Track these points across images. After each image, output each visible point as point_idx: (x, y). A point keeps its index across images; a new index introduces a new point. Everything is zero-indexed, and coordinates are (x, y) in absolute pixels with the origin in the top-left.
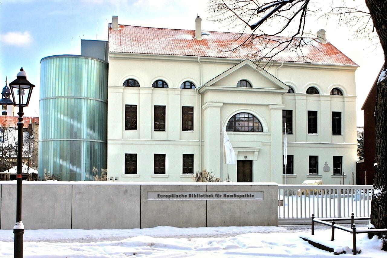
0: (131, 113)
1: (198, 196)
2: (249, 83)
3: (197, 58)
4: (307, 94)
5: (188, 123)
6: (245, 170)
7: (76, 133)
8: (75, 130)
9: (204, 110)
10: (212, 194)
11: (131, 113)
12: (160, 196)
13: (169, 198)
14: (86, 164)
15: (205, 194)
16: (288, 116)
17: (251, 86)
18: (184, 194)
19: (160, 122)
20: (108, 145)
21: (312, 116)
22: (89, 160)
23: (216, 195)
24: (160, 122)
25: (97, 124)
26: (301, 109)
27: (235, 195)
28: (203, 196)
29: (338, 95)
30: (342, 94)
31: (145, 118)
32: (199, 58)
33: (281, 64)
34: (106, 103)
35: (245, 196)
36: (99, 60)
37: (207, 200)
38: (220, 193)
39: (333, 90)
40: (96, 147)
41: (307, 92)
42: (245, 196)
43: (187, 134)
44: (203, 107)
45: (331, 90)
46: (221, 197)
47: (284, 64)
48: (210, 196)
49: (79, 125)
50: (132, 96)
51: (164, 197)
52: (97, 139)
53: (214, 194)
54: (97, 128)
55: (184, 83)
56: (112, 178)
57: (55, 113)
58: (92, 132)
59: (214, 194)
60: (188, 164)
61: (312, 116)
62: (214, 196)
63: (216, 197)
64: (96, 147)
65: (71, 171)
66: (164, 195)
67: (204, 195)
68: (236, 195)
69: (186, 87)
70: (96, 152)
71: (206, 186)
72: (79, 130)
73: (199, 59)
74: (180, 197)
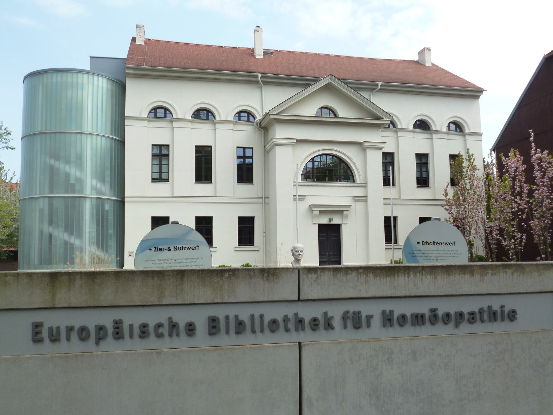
0: (161, 154)
1: (257, 327)
2: (333, 112)
3: (257, 77)
4: (415, 130)
5: (245, 173)
6: (330, 237)
7: (73, 185)
8: (72, 181)
9: (268, 152)
10: (326, 314)
11: (161, 154)
12: (45, 334)
13: (97, 343)
14: (90, 232)
15: (290, 311)
16: (388, 159)
17: (335, 115)
18: (182, 317)
19: (204, 169)
20: (126, 205)
21: (422, 161)
22: (95, 226)
23: (345, 317)
24: (204, 169)
25: (108, 173)
26: (407, 148)
27: (433, 311)
28: (282, 324)
29: (456, 130)
30: (461, 130)
31: (183, 164)
32: (260, 75)
33: (377, 85)
34: (122, 143)
35: (478, 317)
36: (113, 81)
37: (300, 343)
38: (366, 309)
39: (449, 124)
40: (107, 207)
41: (415, 126)
42: (478, 317)
43: (245, 188)
44: (267, 147)
45: (447, 125)
46: (368, 326)
47: (381, 86)
48: (315, 324)
49: (78, 174)
50: (159, 133)
51: (68, 339)
52: (109, 195)
53: (336, 312)
54: (108, 179)
55: (239, 113)
56: (132, 254)
57: (41, 156)
58: (99, 185)
59: (336, 312)
60: (246, 231)
61: (422, 161)
62: (337, 323)
63: (345, 327)
64: (107, 207)
65: (66, 243)
66: (70, 329)
67: (286, 319)
68: (440, 313)
69: (242, 119)
70: (107, 215)
71: (297, 271)
72: (80, 181)
73: (260, 78)
74: (159, 336)
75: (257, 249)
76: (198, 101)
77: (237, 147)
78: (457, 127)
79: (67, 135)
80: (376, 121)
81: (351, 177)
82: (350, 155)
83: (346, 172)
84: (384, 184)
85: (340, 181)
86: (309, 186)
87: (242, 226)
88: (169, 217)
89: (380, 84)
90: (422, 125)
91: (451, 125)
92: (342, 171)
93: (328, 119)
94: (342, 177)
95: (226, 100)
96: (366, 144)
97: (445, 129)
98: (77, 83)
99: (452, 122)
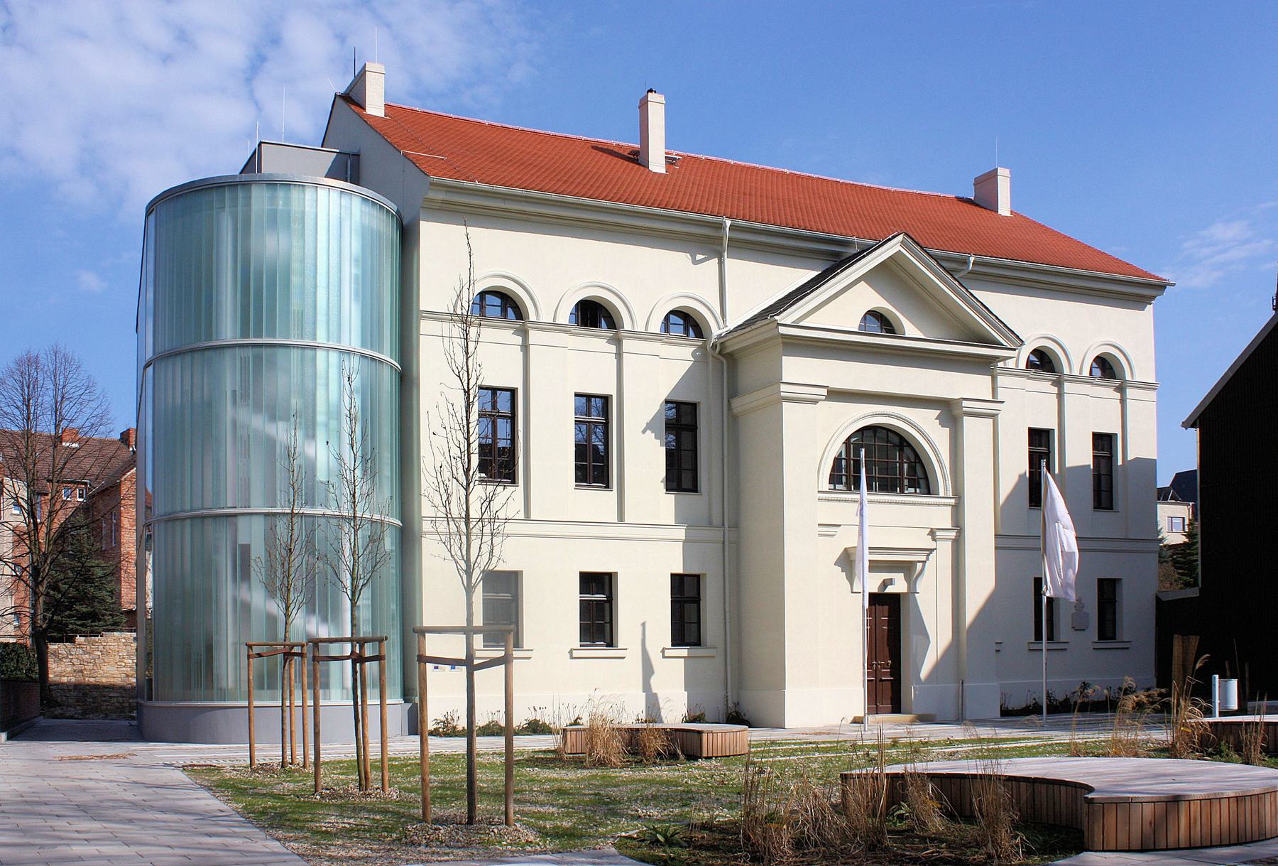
33: (966, 262)
39: (667, 318)
50: (497, 355)
75: (1062, 646)
76: (608, 283)
77: (576, 395)
78: (1106, 367)
79: (281, 351)
80: (976, 348)
81: (922, 482)
82: (926, 429)
83: (912, 469)
84: (1030, 502)
85: (902, 491)
86: (846, 501)
87: (588, 597)
88: (672, 575)
89: (972, 259)
90: (592, 314)
91: (673, 319)
92: (906, 466)
93: (878, 340)
94: (906, 482)
95: (650, 278)
96: (965, 403)
97: (656, 326)
98: (288, 213)
99: (673, 312)
